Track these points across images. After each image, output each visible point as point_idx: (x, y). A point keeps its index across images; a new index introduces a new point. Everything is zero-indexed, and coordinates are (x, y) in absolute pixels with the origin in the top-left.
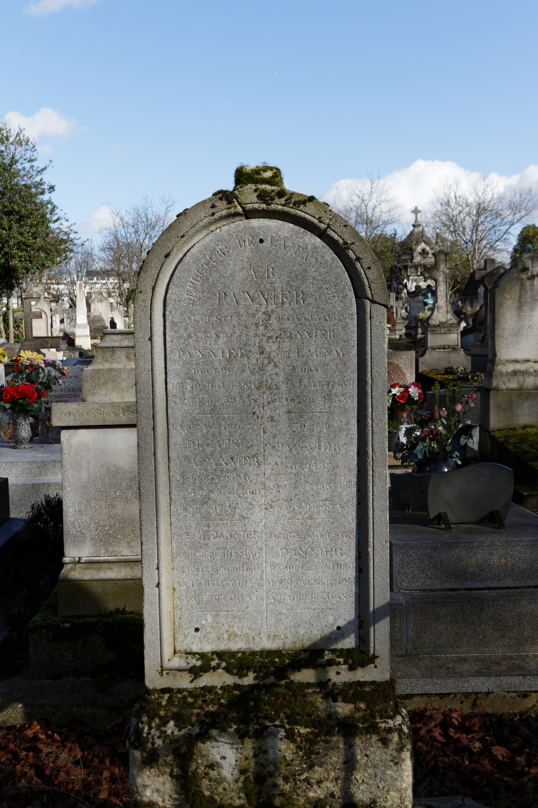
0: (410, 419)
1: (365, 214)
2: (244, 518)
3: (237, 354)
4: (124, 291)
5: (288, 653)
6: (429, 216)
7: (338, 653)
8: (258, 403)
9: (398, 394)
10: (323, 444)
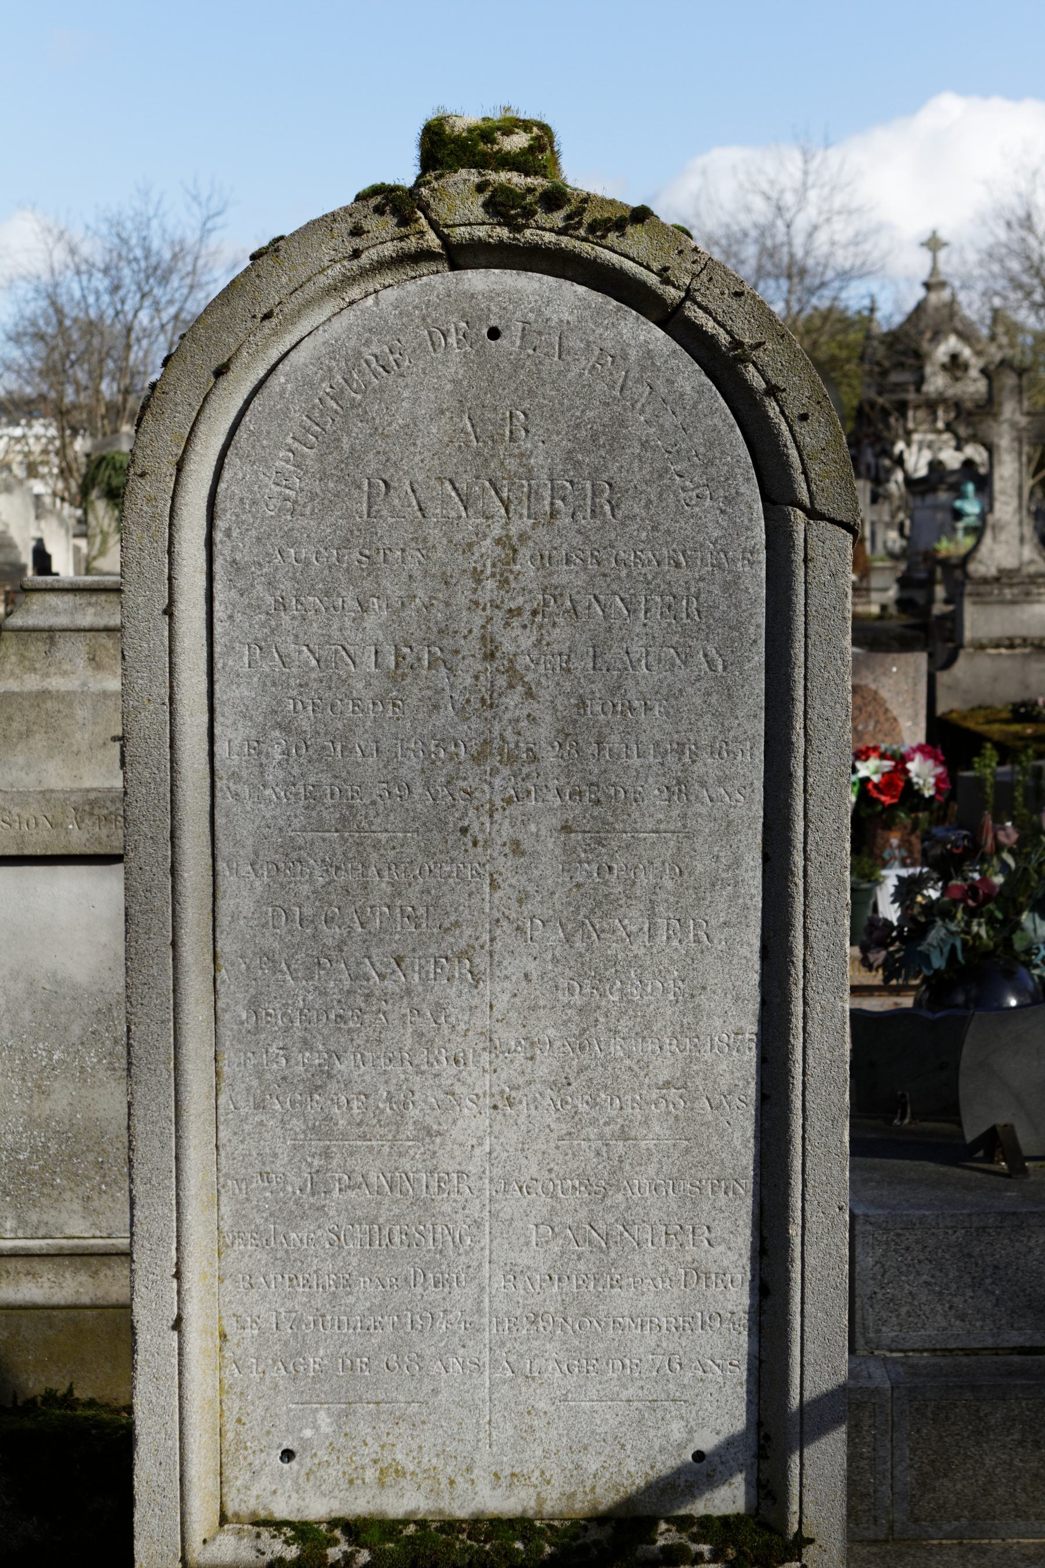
0: (910, 852)
1: (785, 249)
2: (429, 1134)
3: (419, 659)
4: (76, 459)
5: (551, 1527)
6: (972, 257)
7: (695, 1529)
8: (476, 802)
9: (876, 779)
10: (662, 922)
